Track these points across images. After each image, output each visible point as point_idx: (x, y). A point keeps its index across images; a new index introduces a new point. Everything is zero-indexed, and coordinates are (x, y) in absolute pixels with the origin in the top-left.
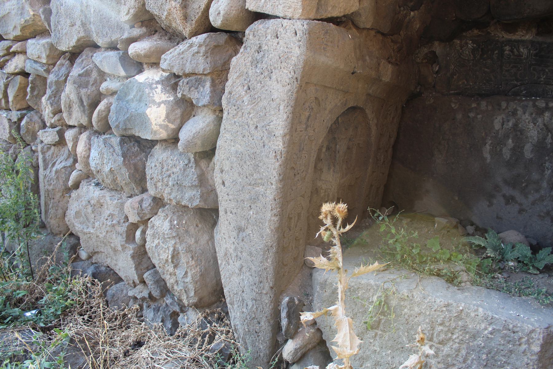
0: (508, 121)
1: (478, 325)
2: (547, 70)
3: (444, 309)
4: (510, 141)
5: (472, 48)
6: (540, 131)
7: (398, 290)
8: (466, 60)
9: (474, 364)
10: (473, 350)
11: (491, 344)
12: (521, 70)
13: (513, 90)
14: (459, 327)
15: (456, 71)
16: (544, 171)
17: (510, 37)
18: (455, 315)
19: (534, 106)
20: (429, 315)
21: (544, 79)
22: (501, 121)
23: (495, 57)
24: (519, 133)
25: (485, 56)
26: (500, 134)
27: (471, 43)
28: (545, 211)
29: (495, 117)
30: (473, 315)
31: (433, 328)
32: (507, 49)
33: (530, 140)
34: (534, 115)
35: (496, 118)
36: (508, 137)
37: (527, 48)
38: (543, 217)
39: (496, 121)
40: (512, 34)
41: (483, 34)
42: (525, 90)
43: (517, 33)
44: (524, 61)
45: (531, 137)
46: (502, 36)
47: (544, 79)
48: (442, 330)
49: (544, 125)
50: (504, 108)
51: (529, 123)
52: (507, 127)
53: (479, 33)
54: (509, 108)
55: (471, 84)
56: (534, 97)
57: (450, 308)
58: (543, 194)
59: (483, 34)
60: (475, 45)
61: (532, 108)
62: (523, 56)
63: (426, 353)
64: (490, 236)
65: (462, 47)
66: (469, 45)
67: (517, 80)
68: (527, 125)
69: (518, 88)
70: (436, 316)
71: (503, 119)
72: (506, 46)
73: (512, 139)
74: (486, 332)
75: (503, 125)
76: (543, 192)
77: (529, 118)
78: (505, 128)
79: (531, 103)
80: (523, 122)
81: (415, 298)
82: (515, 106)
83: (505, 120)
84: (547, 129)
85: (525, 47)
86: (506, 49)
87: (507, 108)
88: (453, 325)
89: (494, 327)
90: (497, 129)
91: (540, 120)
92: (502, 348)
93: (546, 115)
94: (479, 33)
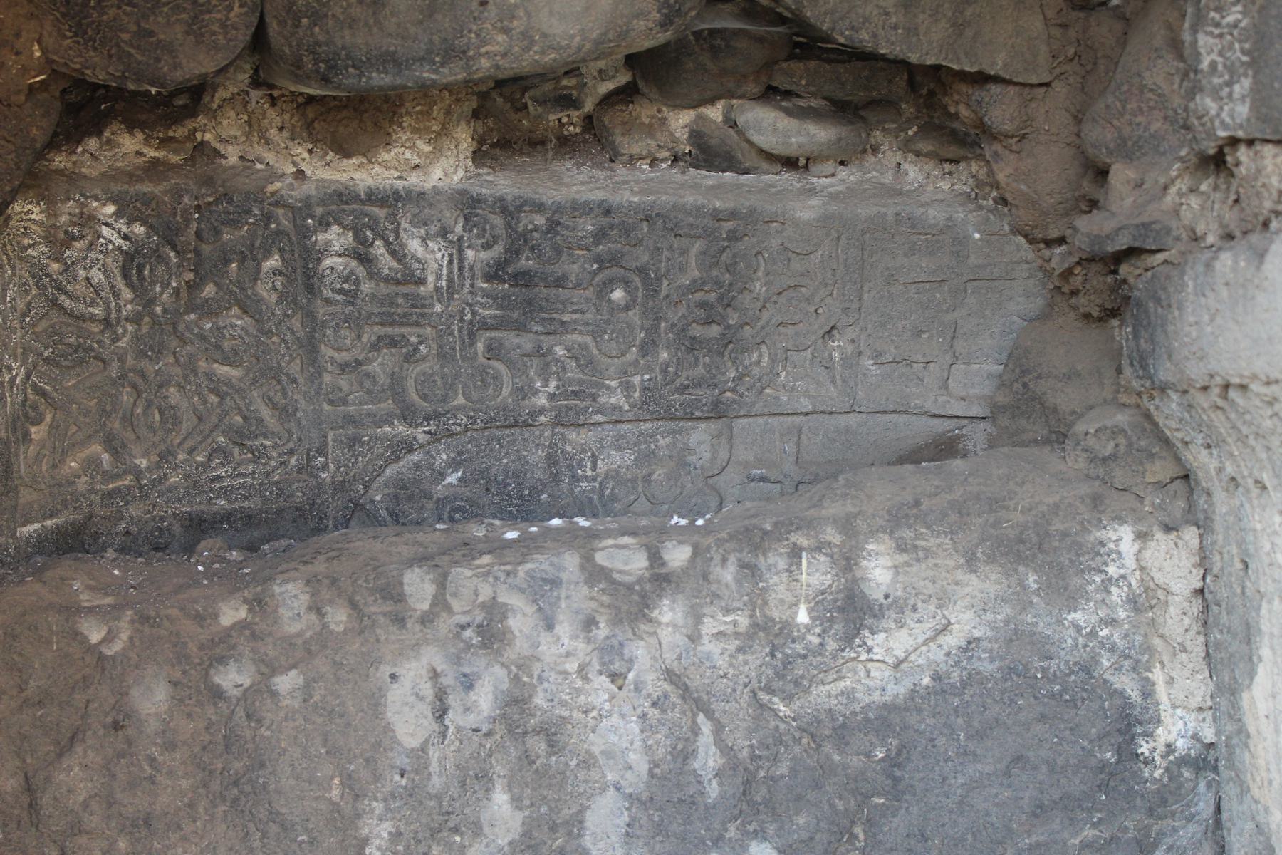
0: (468, 683)
2: (560, 351)
4: (500, 798)
5: (125, 245)
6: (653, 713)
8: (92, 318)
12: (424, 359)
13: (390, 471)
15: (43, 394)
17: (343, 177)
19: (595, 574)
21: (551, 397)
22: (428, 690)
23: (266, 291)
24: (543, 746)
25: (209, 290)
26: (434, 767)
27: (117, 215)
29: (386, 670)
32: (336, 247)
33: (610, 777)
34: (602, 631)
35: (393, 677)
36: (484, 778)
37: (444, 233)
39: (397, 695)
40: (354, 161)
41: (176, 159)
42: (455, 464)
43: (385, 156)
44: (438, 308)
45: (608, 754)
46: (291, 169)
47: (551, 397)
49: (670, 675)
50: (426, 606)
51: (586, 679)
52: (471, 720)
53: (151, 153)
54: (456, 605)
55: (144, 463)
56: (561, 516)
59: (176, 159)
60: (139, 229)
61: (585, 590)
62: (422, 281)
65: (59, 242)
66: (105, 231)
67: (409, 415)
68: (579, 691)
69: (415, 457)
71: (435, 675)
72: (324, 224)
73: (510, 788)
75: (441, 713)
77: (581, 646)
78: (459, 729)
79: (571, 561)
80: (553, 676)
82: (485, 592)
83: (447, 681)
84: (685, 692)
85: (433, 229)
86: (328, 242)
87: (440, 603)
90: (414, 743)
91: (640, 651)
93: (666, 618)
94: (151, 153)
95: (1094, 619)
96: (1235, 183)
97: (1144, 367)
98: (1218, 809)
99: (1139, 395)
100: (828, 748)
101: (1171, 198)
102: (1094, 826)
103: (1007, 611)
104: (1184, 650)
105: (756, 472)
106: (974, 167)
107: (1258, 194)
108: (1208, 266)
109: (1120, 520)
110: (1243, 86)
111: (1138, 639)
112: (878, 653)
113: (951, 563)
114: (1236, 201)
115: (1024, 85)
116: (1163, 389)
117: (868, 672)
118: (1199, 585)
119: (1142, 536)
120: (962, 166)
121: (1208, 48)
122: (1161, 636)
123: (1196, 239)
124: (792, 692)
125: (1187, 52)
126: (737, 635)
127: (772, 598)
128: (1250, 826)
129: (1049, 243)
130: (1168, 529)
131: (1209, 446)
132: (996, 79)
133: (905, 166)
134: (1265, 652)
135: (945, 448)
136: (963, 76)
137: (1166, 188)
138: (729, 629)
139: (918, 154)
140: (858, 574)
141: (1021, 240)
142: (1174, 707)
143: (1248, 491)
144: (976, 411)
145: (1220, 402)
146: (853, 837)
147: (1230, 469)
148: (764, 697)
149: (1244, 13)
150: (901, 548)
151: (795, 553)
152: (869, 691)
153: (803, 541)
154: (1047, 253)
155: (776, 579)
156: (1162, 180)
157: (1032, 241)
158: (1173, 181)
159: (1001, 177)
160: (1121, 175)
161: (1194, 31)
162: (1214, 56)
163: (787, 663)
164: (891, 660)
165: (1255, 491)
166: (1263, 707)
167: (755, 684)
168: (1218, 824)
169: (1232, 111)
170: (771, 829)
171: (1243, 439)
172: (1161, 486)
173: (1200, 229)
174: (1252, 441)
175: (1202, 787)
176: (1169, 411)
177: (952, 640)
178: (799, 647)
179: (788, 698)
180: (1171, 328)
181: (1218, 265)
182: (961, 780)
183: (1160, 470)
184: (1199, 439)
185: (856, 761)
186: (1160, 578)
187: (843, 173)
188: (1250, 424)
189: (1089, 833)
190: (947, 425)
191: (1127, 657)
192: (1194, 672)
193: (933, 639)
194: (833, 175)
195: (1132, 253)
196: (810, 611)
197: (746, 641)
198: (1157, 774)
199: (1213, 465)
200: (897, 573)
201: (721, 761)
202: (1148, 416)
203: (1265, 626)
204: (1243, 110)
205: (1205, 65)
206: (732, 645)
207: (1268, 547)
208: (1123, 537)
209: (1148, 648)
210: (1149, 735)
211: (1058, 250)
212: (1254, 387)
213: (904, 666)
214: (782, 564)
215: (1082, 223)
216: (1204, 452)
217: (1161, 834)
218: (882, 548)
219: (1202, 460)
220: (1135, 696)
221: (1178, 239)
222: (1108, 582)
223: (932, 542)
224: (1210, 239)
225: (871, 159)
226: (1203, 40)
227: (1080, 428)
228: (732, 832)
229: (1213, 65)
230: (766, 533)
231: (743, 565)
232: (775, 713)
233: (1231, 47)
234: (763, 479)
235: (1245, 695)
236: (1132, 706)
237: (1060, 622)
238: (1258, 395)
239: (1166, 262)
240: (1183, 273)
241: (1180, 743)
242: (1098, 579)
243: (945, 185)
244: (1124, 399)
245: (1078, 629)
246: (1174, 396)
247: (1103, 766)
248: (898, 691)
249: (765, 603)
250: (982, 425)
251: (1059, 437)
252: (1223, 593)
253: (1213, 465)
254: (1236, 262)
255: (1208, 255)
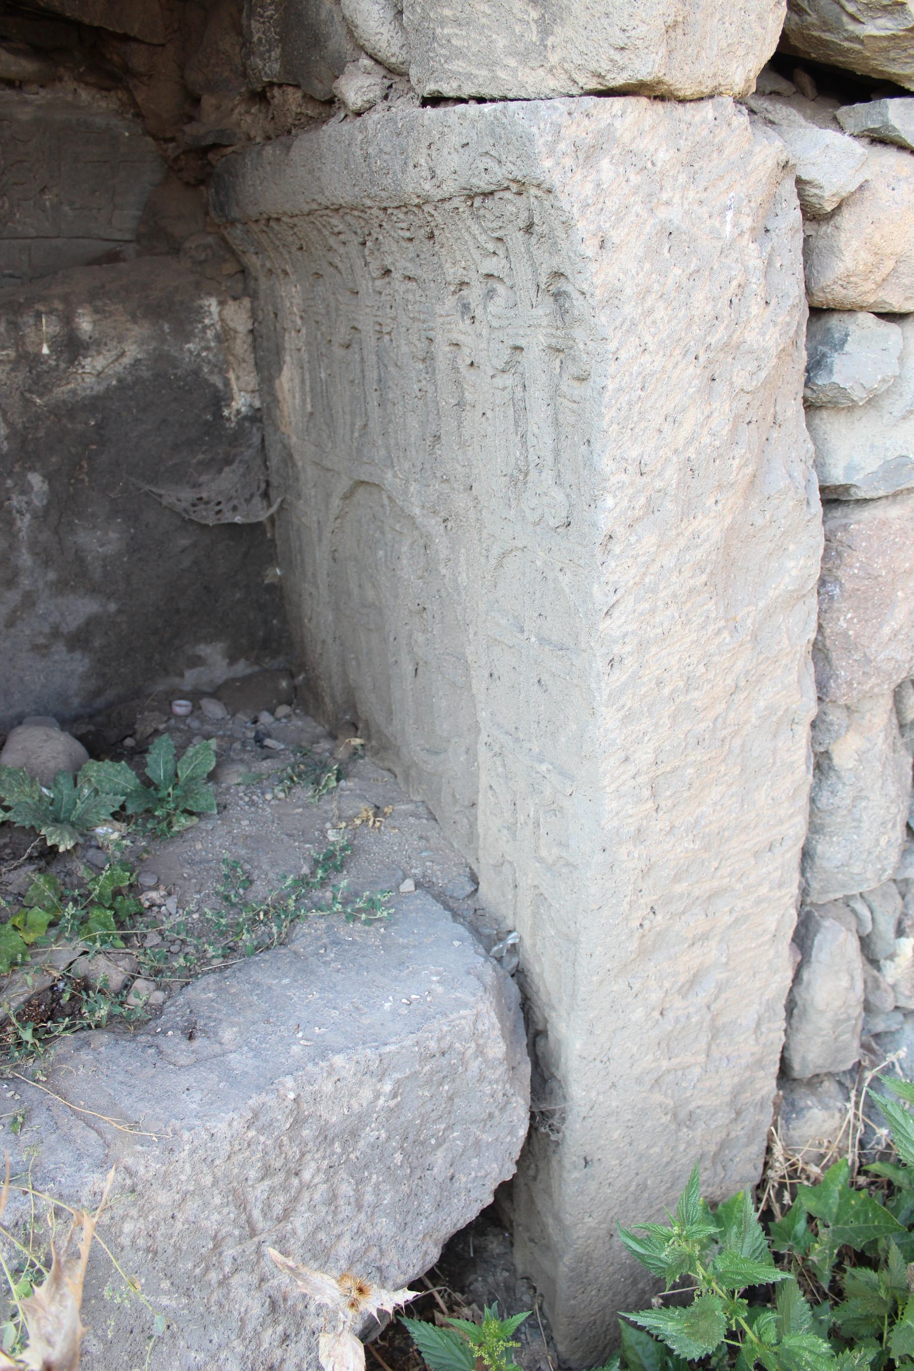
1: (353, 1102)
3: (252, 1133)
7: (66, 1192)
9: (386, 1192)
10: (366, 1167)
11: (402, 1118)
14: (311, 1144)
16: (10, 523)
18: (288, 1126)
20: (215, 1183)
28: (47, 630)
30: (328, 1088)
31: (242, 1205)
38: (46, 647)
48: (272, 1189)
57: (263, 1120)
58: (28, 588)
63: (391, 1311)
64: (7, 786)
70: (236, 1171)
74: (381, 1102)
76: (26, 582)
81: (142, 1170)
88: (293, 1151)
89: (397, 1075)
92: (429, 1107)
95: (199, 347)
96: (271, 108)
97: (222, 210)
98: (263, 440)
99: (219, 226)
100: (64, 421)
101: (235, 116)
102: (203, 453)
103: (154, 344)
104: (244, 361)
105: (7, 272)
106: (120, 94)
107: (285, 114)
108: (259, 154)
109: (210, 294)
110: (276, 53)
111: (221, 357)
112: (88, 369)
113: (123, 319)
114: (273, 118)
115: (150, 44)
116: (233, 223)
117: (83, 379)
118: (251, 327)
119: (221, 303)
120: (112, 93)
121: (258, 31)
122: (233, 355)
123: (250, 139)
124: (45, 390)
125: (245, 31)
126: (10, 362)
127: (27, 340)
128: (280, 446)
129: (167, 140)
130: (235, 299)
131: (257, 253)
132: (135, 40)
133: (79, 91)
134: (288, 358)
135: (113, 257)
136: (114, 35)
137: (232, 110)
138: (5, 358)
139: (87, 84)
140: (74, 326)
141: (149, 139)
142: (240, 391)
143: (278, 276)
144: (128, 237)
145: (265, 228)
146: (82, 467)
147: (268, 265)
148: (28, 395)
149: (276, 10)
150: (96, 311)
151: (38, 315)
152: (84, 389)
153: (42, 309)
154: (165, 146)
155: (28, 330)
156: (230, 106)
157: (156, 138)
158: (236, 106)
159: (139, 100)
160: (208, 101)
161: (249, 19)
162: (260, 34)
163: (39, 376)
164: (95, 372)
165: (282, 276)
166: (286, 386)
167: (22, 388)
168: (263, 447)
169: (270, 67)
170: (38, 465)
171: (276, 248)
172: (230, 276)
173: (252, 134)
174: (281, 249)
175: (254, 430)
176: (235, 235)
177: (126, 361)
178: (45, 367)
179: (41, 396)
180: (238, 188)
181: (264, 153)
182: (135, 434)
183: (230, 267)
184: (252, 249)
185: (80, 427)
186: (232, 325)
187: (43, 92)
188: (280, 239)
189: (200, 457)
190: (112, 245)
191: (216, 366)
192: (250, 372)
193: (116, 360)
194: (37, 93)
195: (215, 146)
196: (49, 347)
197: (16, 365)
198: (233, 425)
199: (259, 264)
200: (95, 325)
201: (7, 431)
202: (223, 239)
203: (287, 345)
204: (277, 67)
205: (255, 39)
206: (8, 367)
207: (288, 305)
208: (212, 304)
209: (226, 361)
210: (229, 406)
211: (172, 145)
212: (285, 219)
213: (102, 375)
214: (31, 321)
215: (187, 128)
216: (254, 257)
217: (235, 456)
218: (86, 311)
219: (253, 261)
220: (220, 386)
221: (240, 139)
222: (206, 327)
223: (113, 307)
224: (258, 140)
225: (58, 85)
226: (254, 24)
227: (187, 245)
228: (17, 468)
229: (260, 39)
230: (21, 305)
231: (9, 322)
232: (35, 403)
233: (269, 30)
234: (11, 276)
235: (277, 382)
236: (219, 391)
237: (182, 349)
238: (286, 223)
239: (233, 152)
240: (244, 158)
241: (243, 409)
242: (200, 326)
243: (104, 104)
244: (209, 229)
245: (191, 352)
246: (239, 226)
247: (206, 422)
248: (100, 388)
249: (24, 343)
250: (132, 245)
251: (176, 250)
252: (264, 331)
253: (259, 264)
254: (274, 151)
255: (257, 148)
